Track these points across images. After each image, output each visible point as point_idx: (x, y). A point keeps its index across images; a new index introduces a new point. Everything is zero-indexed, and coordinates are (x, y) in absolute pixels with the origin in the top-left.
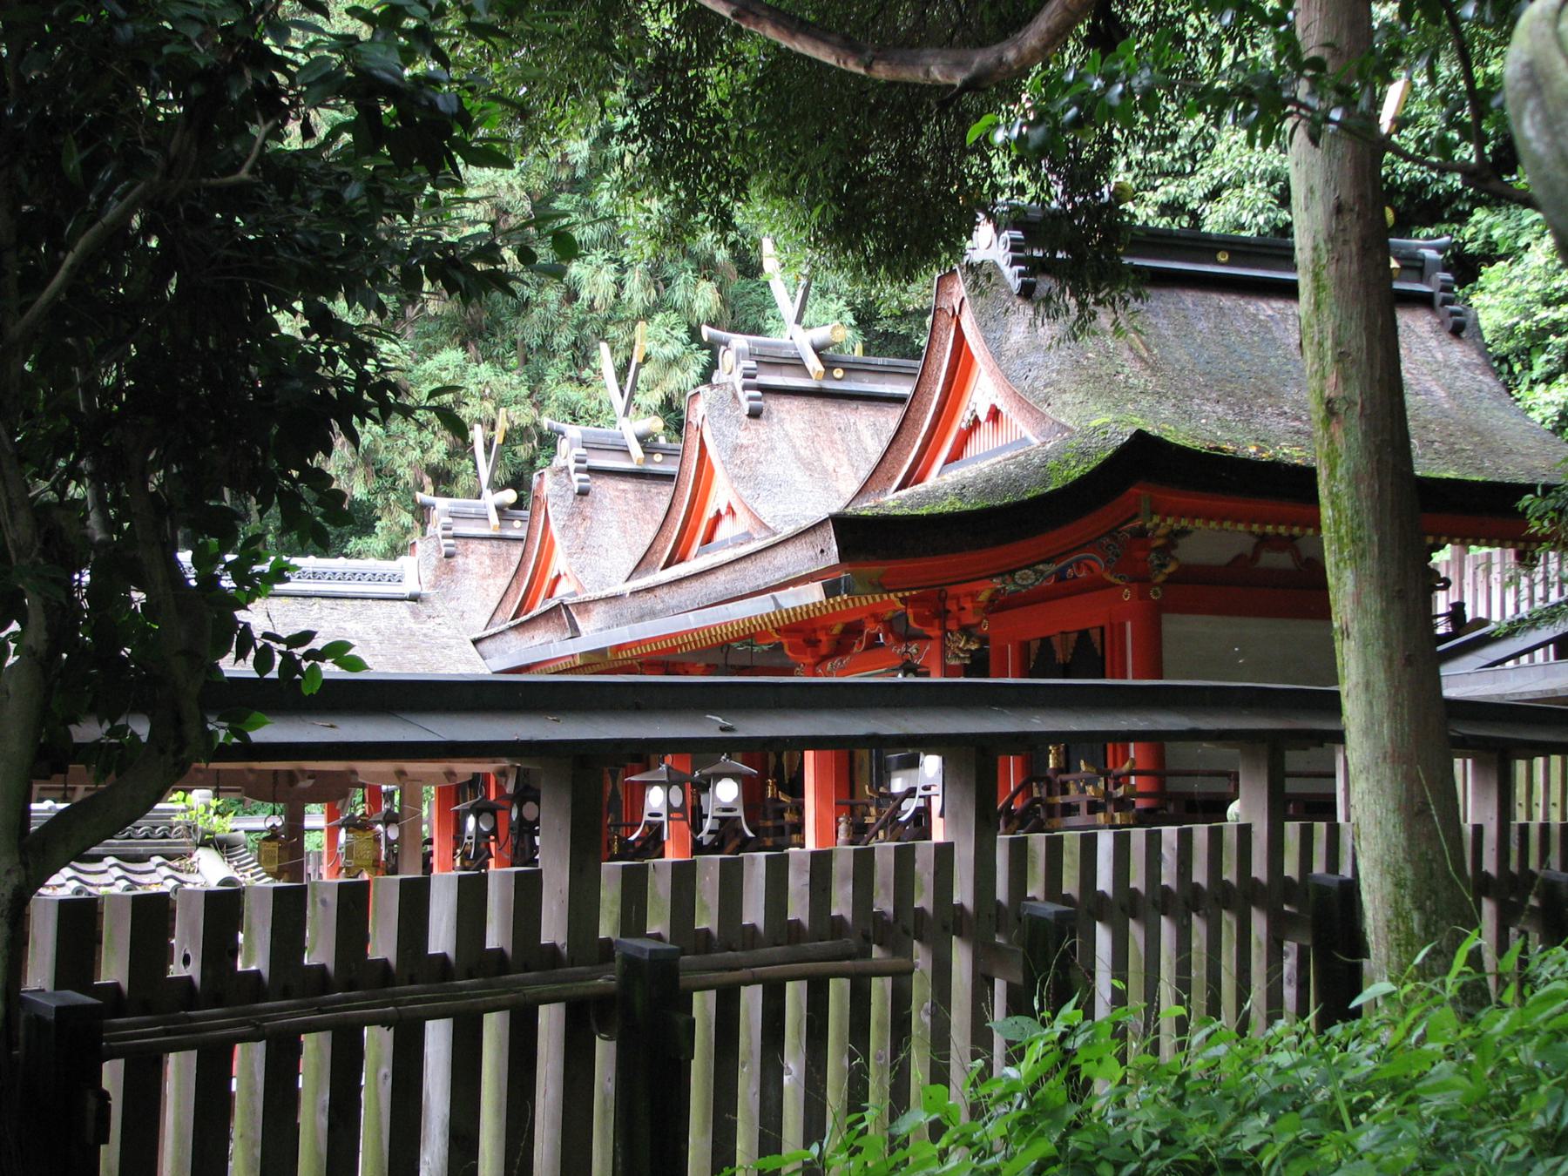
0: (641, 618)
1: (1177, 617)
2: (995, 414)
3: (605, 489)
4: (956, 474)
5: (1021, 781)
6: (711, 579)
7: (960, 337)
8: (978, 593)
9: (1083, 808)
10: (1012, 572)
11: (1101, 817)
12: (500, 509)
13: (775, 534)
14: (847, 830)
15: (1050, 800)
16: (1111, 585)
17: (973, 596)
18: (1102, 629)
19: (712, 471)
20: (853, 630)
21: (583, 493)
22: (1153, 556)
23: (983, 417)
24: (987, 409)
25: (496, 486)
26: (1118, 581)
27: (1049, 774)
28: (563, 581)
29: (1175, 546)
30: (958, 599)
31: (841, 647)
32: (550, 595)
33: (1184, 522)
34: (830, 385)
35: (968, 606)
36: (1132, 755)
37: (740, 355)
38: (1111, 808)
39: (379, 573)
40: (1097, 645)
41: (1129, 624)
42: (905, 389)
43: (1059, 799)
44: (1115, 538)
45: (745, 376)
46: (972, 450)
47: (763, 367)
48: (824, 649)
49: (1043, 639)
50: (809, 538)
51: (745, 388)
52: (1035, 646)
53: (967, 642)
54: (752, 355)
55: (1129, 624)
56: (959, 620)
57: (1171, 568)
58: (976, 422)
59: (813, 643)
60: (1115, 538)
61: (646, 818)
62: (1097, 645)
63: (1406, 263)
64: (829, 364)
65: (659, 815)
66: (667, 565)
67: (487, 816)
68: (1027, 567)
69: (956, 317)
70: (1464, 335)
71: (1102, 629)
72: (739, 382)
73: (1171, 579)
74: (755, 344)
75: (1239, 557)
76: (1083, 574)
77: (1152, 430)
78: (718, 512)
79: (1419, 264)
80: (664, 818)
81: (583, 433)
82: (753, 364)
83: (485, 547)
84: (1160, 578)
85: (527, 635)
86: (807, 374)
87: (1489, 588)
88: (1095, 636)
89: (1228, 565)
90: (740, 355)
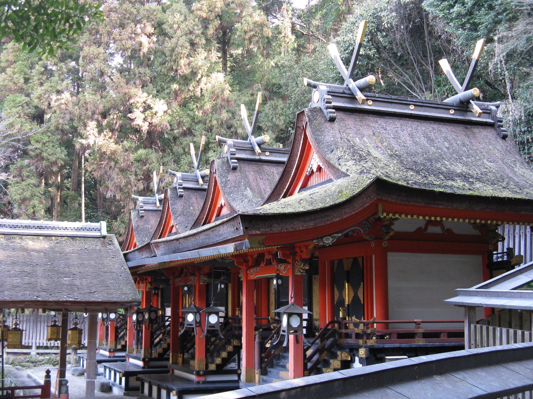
0: (174, 252)
2: (319, 169)
4: (305, 194)
5: (330, 320)
6: (197, 237)
7: (306, 138)
8: (308, 246)
9: (354, 336)
10: (322, 238)
11: (361, 342)
14: (259, 337)
15: (340, 331)
17: (307, 247)
18: (363, 258)
19: (219, 191)
20: (261, 256)
22: (383, 229)
23: (315, 170)
24: (317, 166)
26: (369, 239)
27: (340, 320)
29: (393, 224)
30: (300, 247)
31: (257, 263)
33: (397, 216)
34: (263, 158)
35: (304, 250)
36: (375, 316)
37: (230, 146)
38: (365, 337)
39: (92, 227)
40: (361, 264)
41: (374, 256)
42: (285, 159)
43: (344, 331)
44: (368, 221)
45: (231, 154)
46: (311, 183)
47: (238, 151)
48: (250, 264)
50: (232, 223)
52: (336, 262)
53: (304, 265)
55: (374, 256)
56: (301, 256)
57: (392, 234)
58: (312, 172)
59: (246, 261)
60: (368, 221)
61: (186, 326)
62: (361, 264)
63: (485, 111)
64: (264, 151)
65: (191, 325)
66: (204, 224)
67: (140, 315)
68: (329, 235)
69: (304, 130)
70: (507, 139)
71: (363, 258)
73: (392, 238)
74: (236, 142)
75: (420, 228)
76: (355, 235)
77: (127, 370)
79: (489, 111)
80: (194, 326)
81: (182, 175)
82: (234, 150)
84: (387, 238)
85: (141, 253)
86: (156, 206)
87: (514, 237)
89: (415, 231)
90: (230, 146)
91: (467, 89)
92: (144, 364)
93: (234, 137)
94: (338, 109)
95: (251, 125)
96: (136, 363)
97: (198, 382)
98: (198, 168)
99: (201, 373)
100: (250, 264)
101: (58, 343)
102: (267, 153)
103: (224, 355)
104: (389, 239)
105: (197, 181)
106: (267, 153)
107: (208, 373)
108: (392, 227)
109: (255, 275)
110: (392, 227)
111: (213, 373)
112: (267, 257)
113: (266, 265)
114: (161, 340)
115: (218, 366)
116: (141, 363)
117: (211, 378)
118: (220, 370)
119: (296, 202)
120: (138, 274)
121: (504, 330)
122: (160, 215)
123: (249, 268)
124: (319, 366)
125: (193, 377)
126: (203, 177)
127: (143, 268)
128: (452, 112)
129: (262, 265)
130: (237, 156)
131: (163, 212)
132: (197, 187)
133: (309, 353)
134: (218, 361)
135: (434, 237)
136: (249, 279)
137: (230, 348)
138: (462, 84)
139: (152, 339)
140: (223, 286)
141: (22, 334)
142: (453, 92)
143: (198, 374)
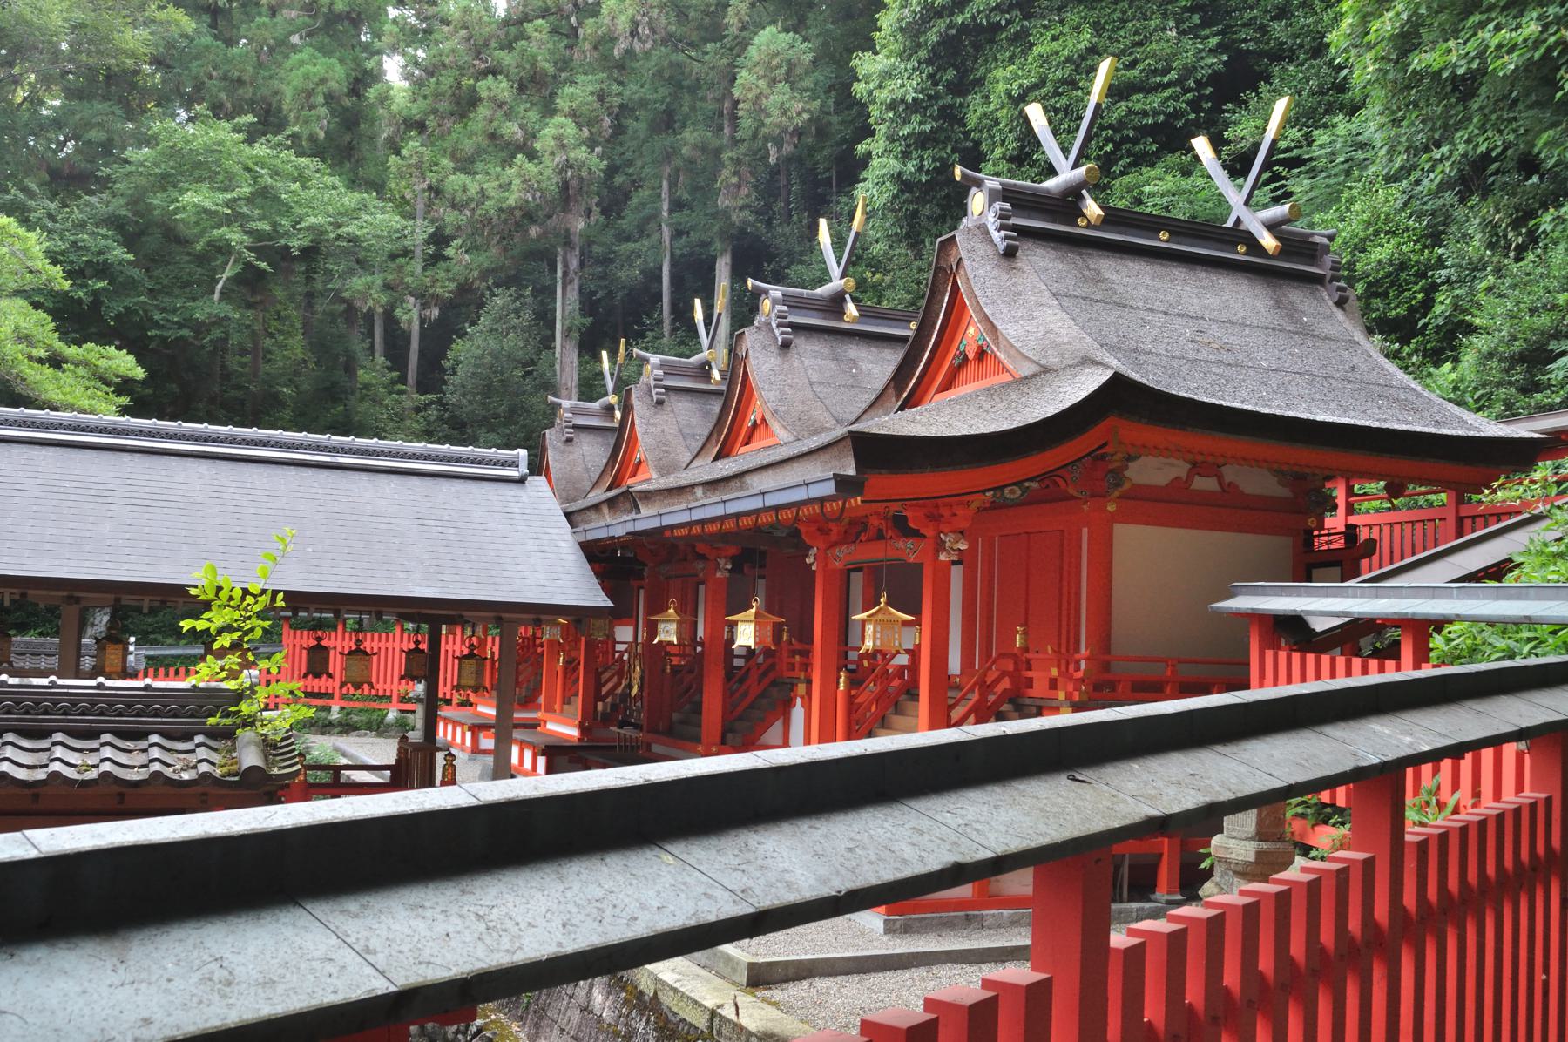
3: (800, 342)
23: (971, 356)
41: (1085, 530)
51: (779, 326)
55: (1085, 530)
57: (1127, 486)
58: (966, 359)
84: (1116, 494)
90: (775, 302)
91: (1076, 165)
95: (839, 263)
101: (420, 688)
108: (1127, 473)
110: (1127, 473)
119: (941, 417)
120: (598, 555)
122: (612, 442)
128: (1164, 236)
130: (792, 319)
131: (620, 431)
135: (1204, 499)
138: (1066, 151)
139: (599, 685)
141: (371, 661)
142: (1051, 171)
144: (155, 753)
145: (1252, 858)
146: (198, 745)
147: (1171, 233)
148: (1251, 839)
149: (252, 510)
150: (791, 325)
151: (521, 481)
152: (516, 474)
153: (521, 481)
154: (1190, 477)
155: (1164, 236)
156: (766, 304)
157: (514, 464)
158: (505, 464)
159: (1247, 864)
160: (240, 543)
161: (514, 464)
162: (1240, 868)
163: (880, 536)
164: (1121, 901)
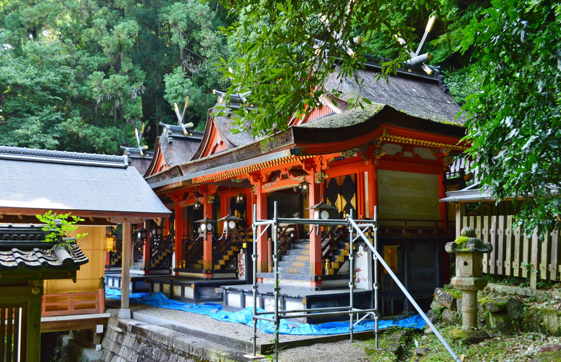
1: (382, 171)
3: (176, 143)
12: (144, 151)
13: (236, 146)
16: (363, 160)
21: (171, 143)
25: (185, 121)
28: (164, 167)
32: (161, 170)
41: (366, 173)
46: (216, 152)
49: (347, 176)
51: (169, 137)
53: (324, 175)
54: (171, 129)
68: (350, 149)
71: (356, 175)
72: (168, 135)
73: (382, 158)
78: (217, 144)
83: (139, 161)
84: (379, 158)
86: (184, 135)
88: (353, 177)
90: (167, 129)
92: (145, 273)
93: (134, 138)
94: (175, 138)
96: (138, 272)
97: (207, 279)
98: (140, 144)
99: (209, 272)
100: (264, 180)
102: (148, 155)
103: (226, 257)
104: (380, 159)
105: (139, 153)
106: (148, 155)
107: (213, 271)
109: (271, 188)
111: (218, 272)
112: (283, 173)
113: (282, 179)
114: (157, 254)
115: (222, 266)
116: (142, 272)
117: (217, 276)
118: (224, 269)
120: (159, 192)
121: (501, 218)
123: (262, 183)
124: (330, 255)
125: (202, 275)
126: (187, 129)
127: (205, 167)
129: (277, 180)
130: (173, 135)
132: (183, 136)
133: (323, 245)
134: (222, 262)
135: (407, 160)
136: (263, 192)
137: (230, 253)
139: (151, 253)
140: (241, 198)
143: (207, 273)
144: (17, 255)
145: (473, 284)
146: (36, 252)
147: (412, 70)
148: (471, 277)
149: (17, 178)
150: (172, 137)
151: (125, 168)
152: (123, 165)
153: (125, 168)
154: (402, 153)
155: (410, 71)
156: (165, 130)
157: (122, 161)
158: (118, 161)
159: (470, 286)
160: (14, 190)
161: (122, 161)
162: (467, 289)
163: (285, 177)
164: (391, 315)
